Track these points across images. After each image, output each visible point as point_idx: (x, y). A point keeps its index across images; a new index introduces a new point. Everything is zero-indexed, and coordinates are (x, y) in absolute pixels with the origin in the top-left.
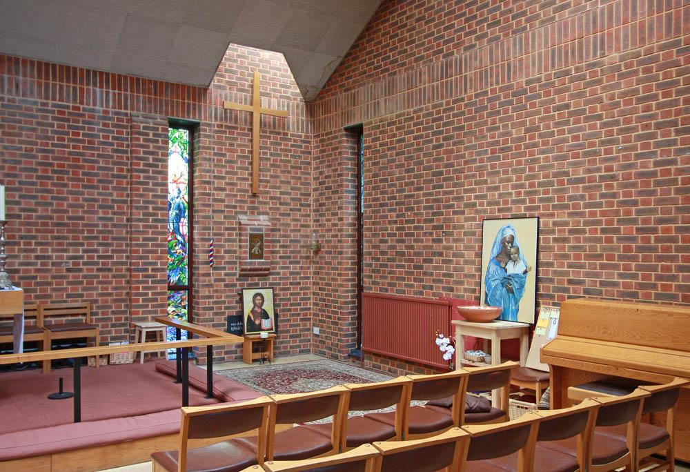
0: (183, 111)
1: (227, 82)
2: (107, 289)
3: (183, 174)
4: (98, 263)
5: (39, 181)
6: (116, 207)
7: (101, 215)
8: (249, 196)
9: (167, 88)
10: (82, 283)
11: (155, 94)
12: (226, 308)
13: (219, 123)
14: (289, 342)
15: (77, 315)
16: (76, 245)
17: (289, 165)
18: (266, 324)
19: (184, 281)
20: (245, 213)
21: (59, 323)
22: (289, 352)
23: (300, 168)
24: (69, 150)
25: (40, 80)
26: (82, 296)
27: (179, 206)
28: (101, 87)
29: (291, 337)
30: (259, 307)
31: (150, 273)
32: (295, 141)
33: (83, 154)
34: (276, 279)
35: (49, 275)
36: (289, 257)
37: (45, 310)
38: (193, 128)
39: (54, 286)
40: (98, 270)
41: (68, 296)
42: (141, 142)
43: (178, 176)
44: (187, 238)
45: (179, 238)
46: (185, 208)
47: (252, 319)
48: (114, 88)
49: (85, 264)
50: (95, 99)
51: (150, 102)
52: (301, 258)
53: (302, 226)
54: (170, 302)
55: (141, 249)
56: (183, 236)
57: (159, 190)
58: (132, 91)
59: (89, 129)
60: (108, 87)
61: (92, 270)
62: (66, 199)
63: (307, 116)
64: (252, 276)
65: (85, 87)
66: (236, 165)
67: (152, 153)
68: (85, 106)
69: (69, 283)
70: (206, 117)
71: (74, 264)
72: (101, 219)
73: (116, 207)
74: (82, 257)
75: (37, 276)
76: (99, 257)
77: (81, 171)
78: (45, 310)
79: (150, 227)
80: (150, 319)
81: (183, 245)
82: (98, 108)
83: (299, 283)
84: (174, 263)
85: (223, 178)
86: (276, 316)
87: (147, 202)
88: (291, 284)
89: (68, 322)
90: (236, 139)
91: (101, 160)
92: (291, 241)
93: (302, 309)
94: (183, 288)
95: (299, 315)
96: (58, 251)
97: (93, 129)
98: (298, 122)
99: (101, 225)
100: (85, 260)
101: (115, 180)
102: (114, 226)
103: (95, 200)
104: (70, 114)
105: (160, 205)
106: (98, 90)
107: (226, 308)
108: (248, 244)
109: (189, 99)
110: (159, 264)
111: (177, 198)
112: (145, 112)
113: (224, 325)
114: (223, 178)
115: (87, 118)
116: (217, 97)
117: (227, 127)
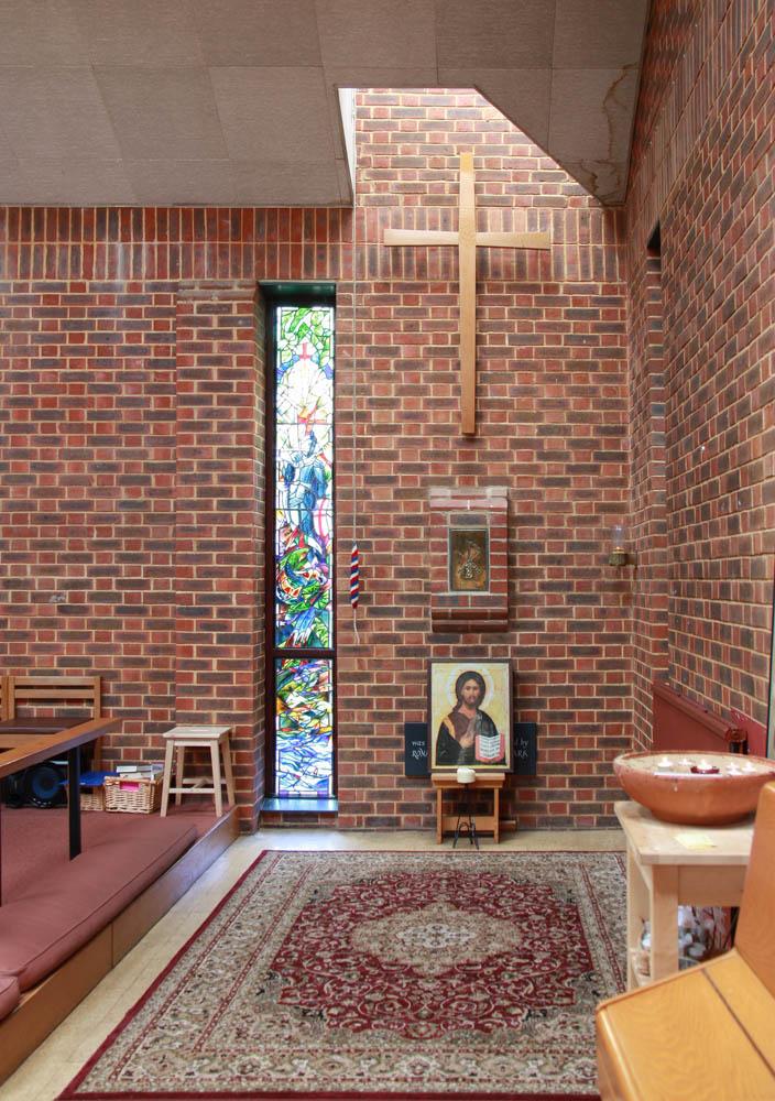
0: (296, 265)
1: (399, 187)
2: (137, 651)
3: (322, 401)
4: (117, 597)
5: (10, 435)
6: (153, 480)
7: (124, 497)
8: (457, 442)
9: (260, 220)
10: (87, 636)
11: (236, 237)
12: (401, 704)
13: (379, 280)
14: (569, 795)
15: (79, 701)
16: (77, 558)
17: (563, 361)
18: (488, 748)
19: (324, 638)
20: (448, 482)
21: (47, 715)
22: (569, 821)
23: (594, 367)
24: (63, 370)
25: (14, 243)
26: (87, 662)
27: (313, 472)
28: (126, 239)
29: (574, 782)
30: (471, 706)
31: (215, 618)
32: (577, 302)
33: (90, 377)
34: (531, 639)
35: (27, 618)
36: (569, 587)
37: (17, 687)
39: (37, 642)
40: (120, 611)
41: (63, 662)
42: (195, 340)
43: (311, 408)
44: (329, 544)
45: (311, 542)
46: (325, 477)
47: (452, 733)
48: (150, 238)
49: (93, 597)
50: (113, 264)
51: (224, 254)
52: (601, 587)
53: (603, 508)
54: (292, 684)
55: (194, 567)
56: (321, 539)
57: (234, 439)
58: (188, 238)
59: (103, 325)
60: (138, 236)
61: (107, 611)
62: (57, 468)
63: (610, 239)
64: (465, 630)
65: (95, 244)
66: (422, 373)
67: (218, 361)
68: (95, 281)
69: (64, 636)
70: (346, 268)
71: (75, 598)
72: (123, 505)
73: (153, 480)
74: (87, 584)
75: (6, 620)
76: (121, 584)
77: (86, 411)
78: (17, 687)
79: (214, 519)
80: (214, 720)
81: (322, 560)
82: (118, 281)
83: (596, 651)
84: (301, 599)
85: (393, 403)
86: (522, 732)
87: (208, 466)
88: (573, 651)
89: (62, 715)
90: (423, 312)
91: (123, 385)
92: (571, 547)
93: (604, 717)
95: (595, 729)
96: (43, 571)
97: (108, 325)
98: (585, 255)
99: (123, 519)
100: (94, 590)
101: (152, 424)
102: (150, 519)
103: (113, 468)
104: (67, 299)
105: (235, 471)
106: (119, 245)
107: (401, 704)
108: (448, 554)
109: (309, 235)
110: (234, 600)
111: (309, 455)
112: (214, 276)
113: (397, 743)
114: (393, 403)
115: (97, 305)
116: (375, 224)
117: (400, 287)
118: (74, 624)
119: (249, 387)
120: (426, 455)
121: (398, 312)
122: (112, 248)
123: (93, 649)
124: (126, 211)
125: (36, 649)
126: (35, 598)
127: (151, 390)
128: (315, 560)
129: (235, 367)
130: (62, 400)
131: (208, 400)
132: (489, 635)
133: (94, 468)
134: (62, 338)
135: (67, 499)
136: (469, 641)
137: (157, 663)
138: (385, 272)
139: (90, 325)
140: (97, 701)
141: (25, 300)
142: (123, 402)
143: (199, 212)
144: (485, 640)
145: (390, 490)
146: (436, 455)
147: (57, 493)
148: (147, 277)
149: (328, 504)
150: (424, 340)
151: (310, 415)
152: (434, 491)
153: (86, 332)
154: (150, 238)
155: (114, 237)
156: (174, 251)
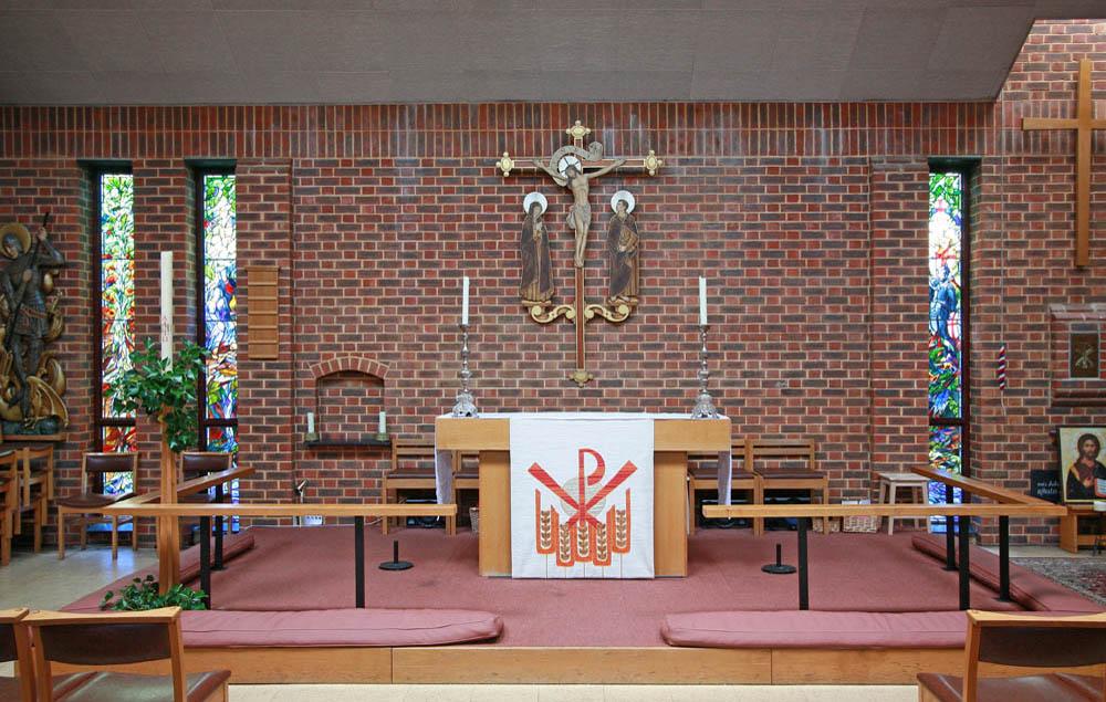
0: (953, 145)
1: (1029, 85)
3: (954, 242)
7: (828, 313)
11: (908, 123)
12: (1028, 457)
13: (1014, 155)
19: (955, 411)
20: (1063, 300)
26: (802, 429)
30: (1090, 459)
37: (755, 447)
38: (968, 169)
40: (826, 393)
41: (785, 429)
43: (945, 247)
45: (947, 343)
47: (1078, 478)
49: (806, 383)
50: (818, 145)
54: (933, 443)
56: (952, 340)
58: (872, 124)
61: (817, 393)
64: (1076, 405)
68: (805, 157)
70: (993, 147)
71: (793, 384)
72: (828, 318)
76: (827, 374)
77: (800, 251)
78: (755, 447)
80: (901, 469)
82: (823, 157)
85: (1023, 244)
91: (827, 232)
94: (953, 422)
96: (771, 365)
101: (848, 260)
102: (846, 328)
103: (820, 292)
104: (784, 170)
106: (822, 130)
107: (1028, 457)
108: (1069, 351)
109: (962, 122)
111: (944, 281)
114: (1023, 244)
115: (807, 174)
117: (1028, 160)
118: (792, 402)
119: (182, 237)
120: (1046, 281)
121: (1027, 178)
122: (818, 133)
123: (806, 420)
124: (827, 106)
125: (766, 420)
126: (765, 384)
127: (848, 235)
128: (949, 355)
129: (916, 219)
130: (783, 243)
131: (896, 244)
132: (1091, 408)
133: (806, 291)
134: (782, 199)
135: (786, 314)
136: (1078, 413)
137: (852, 429)
138: (1018, 149)
139: (54, 182)
140: (812, 457)
141: (755, 171)
142: (827, 244)
143: (881, 106)
144: (1090, 412)
145: (1020, 306)
146: (1054, 281)
147: (780, 309)
148: (843, 154)
149: (958, 316)
150: (1047, 198)
151: (945, 252)
152: (1054, 306)
153: (800, 194)
154: (845, 125)
155: (818, 125)
156: (863, 134)
